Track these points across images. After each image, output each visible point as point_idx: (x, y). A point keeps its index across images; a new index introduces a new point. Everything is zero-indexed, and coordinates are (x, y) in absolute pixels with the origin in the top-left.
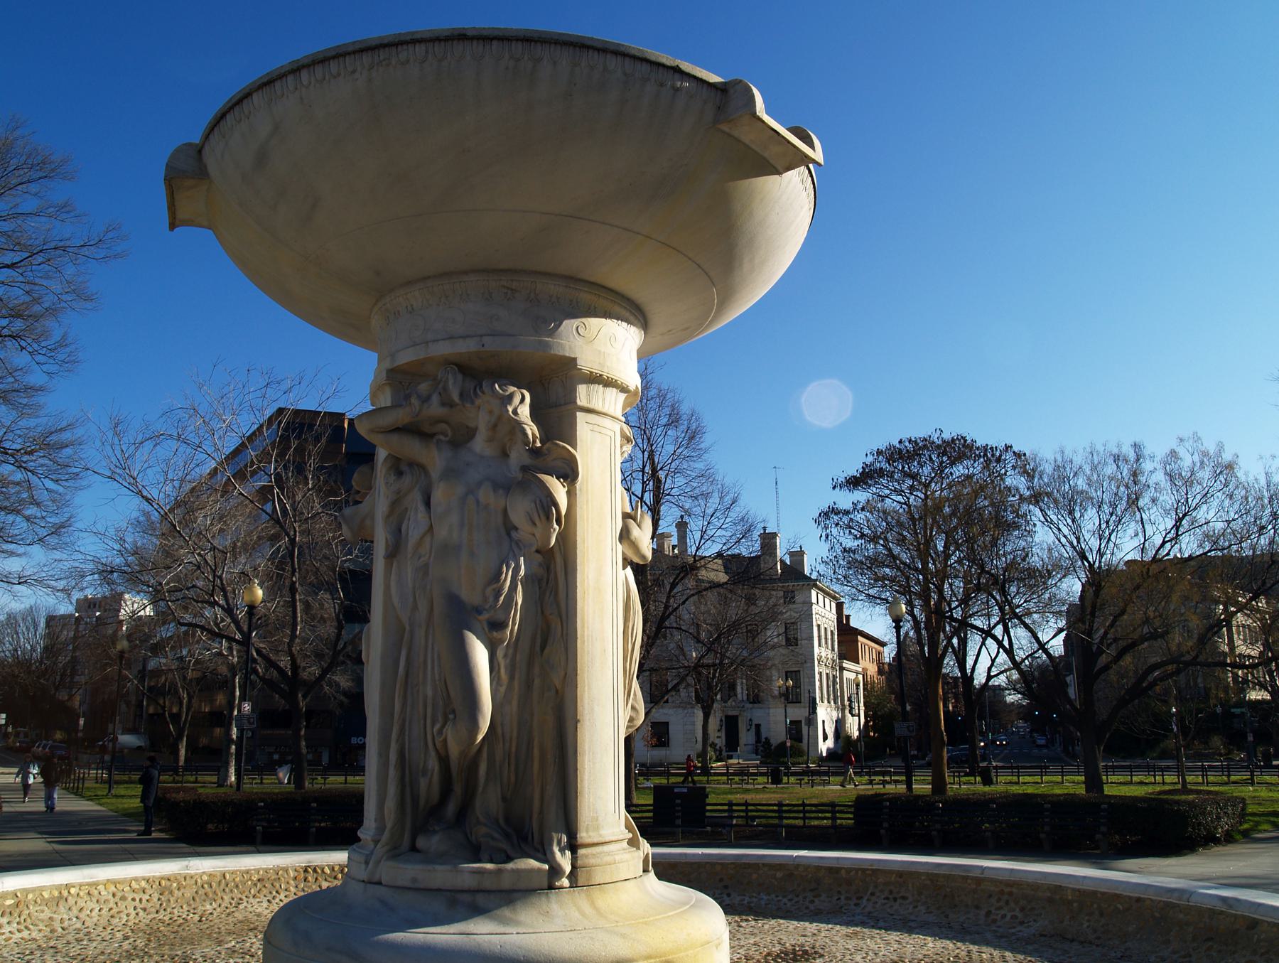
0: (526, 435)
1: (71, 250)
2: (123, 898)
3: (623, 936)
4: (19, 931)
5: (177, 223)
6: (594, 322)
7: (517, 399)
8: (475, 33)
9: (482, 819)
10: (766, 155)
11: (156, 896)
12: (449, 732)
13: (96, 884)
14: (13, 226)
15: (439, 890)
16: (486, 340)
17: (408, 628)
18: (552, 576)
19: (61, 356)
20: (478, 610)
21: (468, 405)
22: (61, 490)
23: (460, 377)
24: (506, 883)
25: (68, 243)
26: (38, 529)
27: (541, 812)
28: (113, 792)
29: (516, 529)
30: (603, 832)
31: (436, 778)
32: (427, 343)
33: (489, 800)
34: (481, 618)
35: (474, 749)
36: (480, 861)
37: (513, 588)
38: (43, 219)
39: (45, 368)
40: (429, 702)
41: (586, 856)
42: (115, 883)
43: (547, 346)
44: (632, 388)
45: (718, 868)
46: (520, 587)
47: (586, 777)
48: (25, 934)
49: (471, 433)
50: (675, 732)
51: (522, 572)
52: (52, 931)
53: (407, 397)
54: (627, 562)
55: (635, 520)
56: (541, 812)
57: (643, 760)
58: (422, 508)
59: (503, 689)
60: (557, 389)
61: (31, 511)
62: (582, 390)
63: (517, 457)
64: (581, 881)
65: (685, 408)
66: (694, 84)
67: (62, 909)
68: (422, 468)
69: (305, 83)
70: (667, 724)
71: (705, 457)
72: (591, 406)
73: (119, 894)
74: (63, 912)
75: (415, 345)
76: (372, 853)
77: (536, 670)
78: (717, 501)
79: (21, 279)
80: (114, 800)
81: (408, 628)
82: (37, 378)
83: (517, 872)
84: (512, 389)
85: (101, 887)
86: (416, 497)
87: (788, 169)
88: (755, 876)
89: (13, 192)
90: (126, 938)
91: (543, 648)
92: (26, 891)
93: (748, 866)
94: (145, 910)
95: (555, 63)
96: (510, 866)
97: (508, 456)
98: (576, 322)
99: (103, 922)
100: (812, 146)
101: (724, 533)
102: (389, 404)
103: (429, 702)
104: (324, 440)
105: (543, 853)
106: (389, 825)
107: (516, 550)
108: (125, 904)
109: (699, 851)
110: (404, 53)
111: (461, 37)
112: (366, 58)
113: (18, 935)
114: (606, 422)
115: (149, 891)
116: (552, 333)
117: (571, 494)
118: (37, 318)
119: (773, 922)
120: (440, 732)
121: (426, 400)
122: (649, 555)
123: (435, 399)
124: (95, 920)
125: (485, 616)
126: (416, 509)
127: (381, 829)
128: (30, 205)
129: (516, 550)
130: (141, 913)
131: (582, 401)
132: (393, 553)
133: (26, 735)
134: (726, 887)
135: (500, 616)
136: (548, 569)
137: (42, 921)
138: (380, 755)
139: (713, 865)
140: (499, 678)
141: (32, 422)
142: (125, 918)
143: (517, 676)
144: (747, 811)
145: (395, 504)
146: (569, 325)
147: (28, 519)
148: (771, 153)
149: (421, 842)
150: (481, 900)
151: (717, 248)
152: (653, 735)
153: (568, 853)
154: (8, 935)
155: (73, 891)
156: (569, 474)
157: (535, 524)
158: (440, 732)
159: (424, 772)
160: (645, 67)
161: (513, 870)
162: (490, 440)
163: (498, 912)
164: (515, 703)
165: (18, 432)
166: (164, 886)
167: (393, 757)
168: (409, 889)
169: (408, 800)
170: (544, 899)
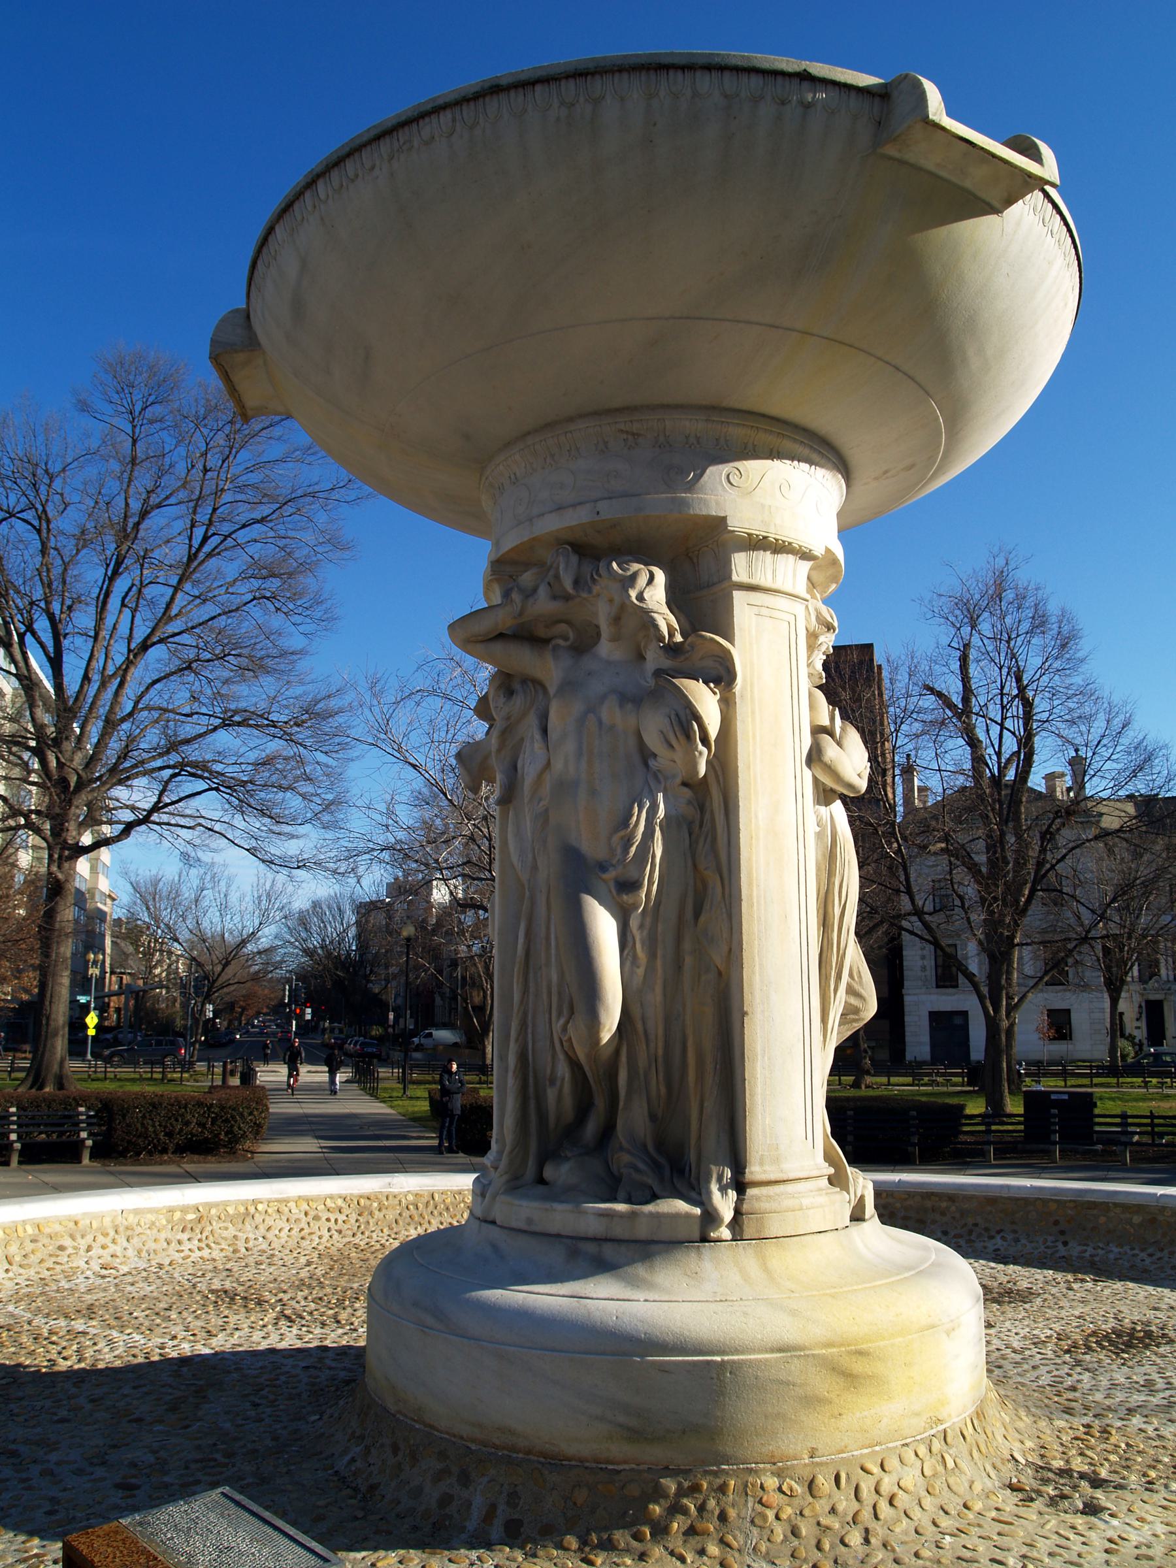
0: (656, 627)
1: (321, 495)
2: (317, 1218)
3: (794, 1313)
4: (200, 1249)
5: (250, 413)
6: (753, 468)
7: (643, 580)
8: (510, 80)
9: (625, 1144)
10: (968, 184)
11: (354, 1216)
13: (286, 1201)
14: (261, 476)
15: (558, 1236)
16: (602, 506)
18: (707, 816)
19: (318, 614)
20: (603, 867)
22: (334, 763)
23: (574, 559)
24: (642, 1231)
25: (317, 488)
26: (312, 806)
27: (699, 1137)
28: (408, 1093)
29: (655, 756)
30: (786, 1166)
31: (567, 1088)
33: (635, 1119)
34: (605, 876)
36: (614, 1200)
37: (649, 834)
38: (291, 465)
39: (301, 629)
40: (554, 990)
41: (758, 1198)
42: (308, 1200)
43: (684, 503)
44: (819, 551)
45: (1053, 1206)
46: (658, 834)
47: (759, 1090)
48: (205, 1253)
50: (1080, 1021)
51: (661, 813)
52: (235, 1251)
54: (824, 795)
55: (831, 734)
57: (1035, 1056)
58: (538, 736)
59: (640, 971)
60: (703, 568)
61: (307, 788)
63: (654, 659)
64: (748, 1232)
65: (1052, 608)
66: (834, 93)
67: (248, 1227)
69: (323, 197)
70: (1068, 1012)
71: (1084, 668)
73: (312, 1213)
74: (249, 1231)
77: (687, 945)
78: (1104, 724)
79: (272, 534)
80: (407, 1103)
82: (295, 641)
83: (658, 1216)
84: (636, 566)
85: (292, 1205)
86: (531, 724)
87: (1010, 201)
88: (1102, 1219)
89: (257, 439)
90: (309, 1264)
91: (697, 915)
92: (210, 1206)
93: (1093, 1205)
94: (340, 1232)
95: (622, 99)
96: (649, 1208)
98: (725, 468)
99: (292, 1244)
100: (1037, 157)
101: (1115, 765)
103: (554, 990)
105: (696, 1193)
106: (508, 1148)
108: (318, 1224)
109: (1027, 1182)
110: (427, 128)
111: (495, 89)
112: (385, 146)
113: (198, 1253)
115: (346, 1211)
116: (691, 487)
117: (727, 704)
118: (290, 575)
119: (1119, 1285)
120: (564, 1029)
122: (863, 785)
123: (543, 591)
124: (283, 1241)
125: (611, 875)
126: (532, 737)
128: (275, 451)
130: (336, 1235)
133: (341, 1031)
134: (1062, 1233)
135: (633, 874)
136: (702, 808)
137: (225, 1239)
139: (1045, 1202)
141: (298, 690)
142: (317, 1240)
143: (660, 953)
144: (1152, 1125)
146: (716, 473)
147: (304, 796)
148: (975, 179)
149: (549, 1172)
150: (608, 1251)
151: (923, 345)
152: (1051, 1025)
153: (732, 1195)
154: (187, 1253)
155: (260, 1207)
156: (721, 675)
157: (671, 746)
158: (564, 1029)
160: (755, 81)
161: (651, 1214)
164: (659, 989)
165: (285, 702)
166: (363, 1206)
168: (525, 1232)
169: (533, 1117)
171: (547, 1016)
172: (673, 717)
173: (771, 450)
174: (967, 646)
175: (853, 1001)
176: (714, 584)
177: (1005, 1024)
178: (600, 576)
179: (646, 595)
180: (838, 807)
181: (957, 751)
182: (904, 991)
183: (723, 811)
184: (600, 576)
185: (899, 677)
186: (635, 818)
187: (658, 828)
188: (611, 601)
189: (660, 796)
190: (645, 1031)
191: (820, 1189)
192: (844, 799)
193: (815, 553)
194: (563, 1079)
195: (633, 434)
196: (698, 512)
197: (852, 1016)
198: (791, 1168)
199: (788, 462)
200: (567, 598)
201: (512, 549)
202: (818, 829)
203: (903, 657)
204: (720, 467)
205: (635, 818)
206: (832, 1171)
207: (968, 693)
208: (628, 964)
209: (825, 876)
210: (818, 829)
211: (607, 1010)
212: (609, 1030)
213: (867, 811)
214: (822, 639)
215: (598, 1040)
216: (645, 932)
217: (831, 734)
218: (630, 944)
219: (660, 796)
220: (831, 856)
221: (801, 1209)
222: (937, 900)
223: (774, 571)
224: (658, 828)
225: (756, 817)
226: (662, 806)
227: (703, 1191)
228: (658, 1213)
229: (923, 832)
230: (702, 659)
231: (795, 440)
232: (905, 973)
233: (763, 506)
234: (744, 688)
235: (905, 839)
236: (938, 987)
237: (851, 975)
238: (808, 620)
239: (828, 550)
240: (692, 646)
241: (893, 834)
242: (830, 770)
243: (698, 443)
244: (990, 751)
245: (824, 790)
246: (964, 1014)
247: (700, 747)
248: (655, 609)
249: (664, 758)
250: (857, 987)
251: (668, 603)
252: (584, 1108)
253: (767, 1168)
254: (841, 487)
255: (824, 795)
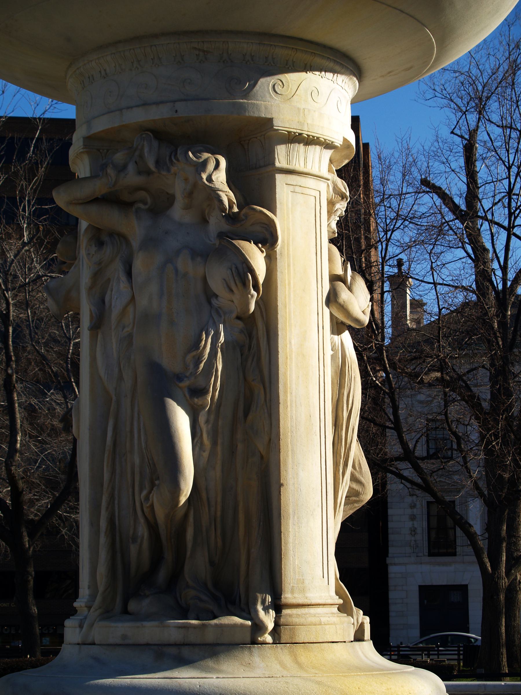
0: (221, 202)
6: (292, 78)
7: (211, 166)
12: (155, 498)
15: (148, 645)
17: (114, 398)
18: (254, 342)
20: (179, 378)
21: (164, 173)
23: (155, 143)
24: (210, 637)
27: (247, 575)
29: (216, 296)
31: (146, 545)
32: (121, 110)
33: (198, 564)
34: (182, 384)
35: (180, 514)
40: (137, 470)
41: (290, 616)
43: (242, 108)
44: (338, 142)
46: (219, 354)
49: (171, 200)
51: (222, 339)
53: (104, 167)
54: (337, 327)
55: (344, 281)
56: (247, 575)
58: (123, 278)
59: (206, 454)
60: (256, 155)
62: (281, 150)
63: (216, 224)
64: (285, 637)
68: (123, 238)
72: (291, 167)
75: (110, 112)
76: (86, 618)
81: (114, 398)
83: (221, 626)
84: (206, 155)
91: (246, 414)
97: (208, 222)
98: (272, 80)
102: (88, 175)
103: (137, 470)
104: (42, 170)
106: (101, 589)
107: (215, 317)
114: (310, 182)
116: (247, 94)
117: (271, 260)
120: (147, 498)
121: (122, 169)
122: (366, 319)
123: (131, 167)
125: (185, 384)
127: (93, 597)
129: (215, 317)
131: (281, 162)
132: (98, 324)
135: (201, 383)
136: (250, 336)
138: (92, 524)
140: (202, 443)
143: (220, 441)
145: (96, 275)
146: (265, 83)
150: (186, 652)
153: (272, 613)
156: (267, 238)
157: (231, 291)
158: (147, 498)
159: (134, 539)
161: (216, 625)
162: (187, 207)
163: (202, 663)
164: (218, 468)
167: (103, 524)
168: (120, 645)
170: (246, 653)
171: (131, 490)
172: (234, 269)
173: (306, 65)
174: (473, 133)
175: (355, 486)
176: (260, 167)
177: (505, 582)
178: (178, 160)
179: (214, 178)
180: (346, 336)
181: (457, 265)
182: (389, 561)
183: (265, 339)
184: (178, 160)
185: (392, 178)
186: (203, 342)
187: (219, 350)
188: (186, 180)
189: (221, 326)
190: (208, 499)
191: (333, 613)
192: (351, 329)
193: (336, 144)
194: (143, 537)
195: (204, 51)
196: (252, 114)
197: (354, 498)
198: (313, 597)
199: (317, 73)
200: (148, 173)
201: (103, 131)
202: (332, 353)
203: (396, 155)
204: (268, 79)
205: (203, 342)
206: (341, 601)
207: (472, 196)
208: (197, 449)
209: (337, 388)
210: (332, 353)
211: (185, 480)
212: (186, 495)
213: (366, 338)
214: (338, 206)
215: (178, 502)
216: (210, 426)
217: (344, 281)
218: (199, 435)
219: (221, 326)
220: (341, 374)
221: (320, 624)
222: (432, 445)
223: (305, 159)
224: (219, 350)
225: (290, 343)
226: (222, 334)
227: (252, 610)
228: (221, 624)
229: (415, 358)
230: (253, 224)
231: (323, 57)
232: (391, 537)
233: (299, 109)
234: (283, 247)
235: (393, 365)
236: (430, 554)
237: (354, 466)
238: (328, 192)
239: (345, 140)
240: (246, 216)
241: (379, 360)
242: (344, 309)
243: (252, 60)
244: (495, 265)
245: (337, 323)
246: (463, 589)
247: (253, 292)
248: (220, 188)
249: (224, 298)
250: (357, 475)
251: (227, 182)
252: (157, 558)
253: (296, 595)
254: (355, 86)
255: (337, 327)
